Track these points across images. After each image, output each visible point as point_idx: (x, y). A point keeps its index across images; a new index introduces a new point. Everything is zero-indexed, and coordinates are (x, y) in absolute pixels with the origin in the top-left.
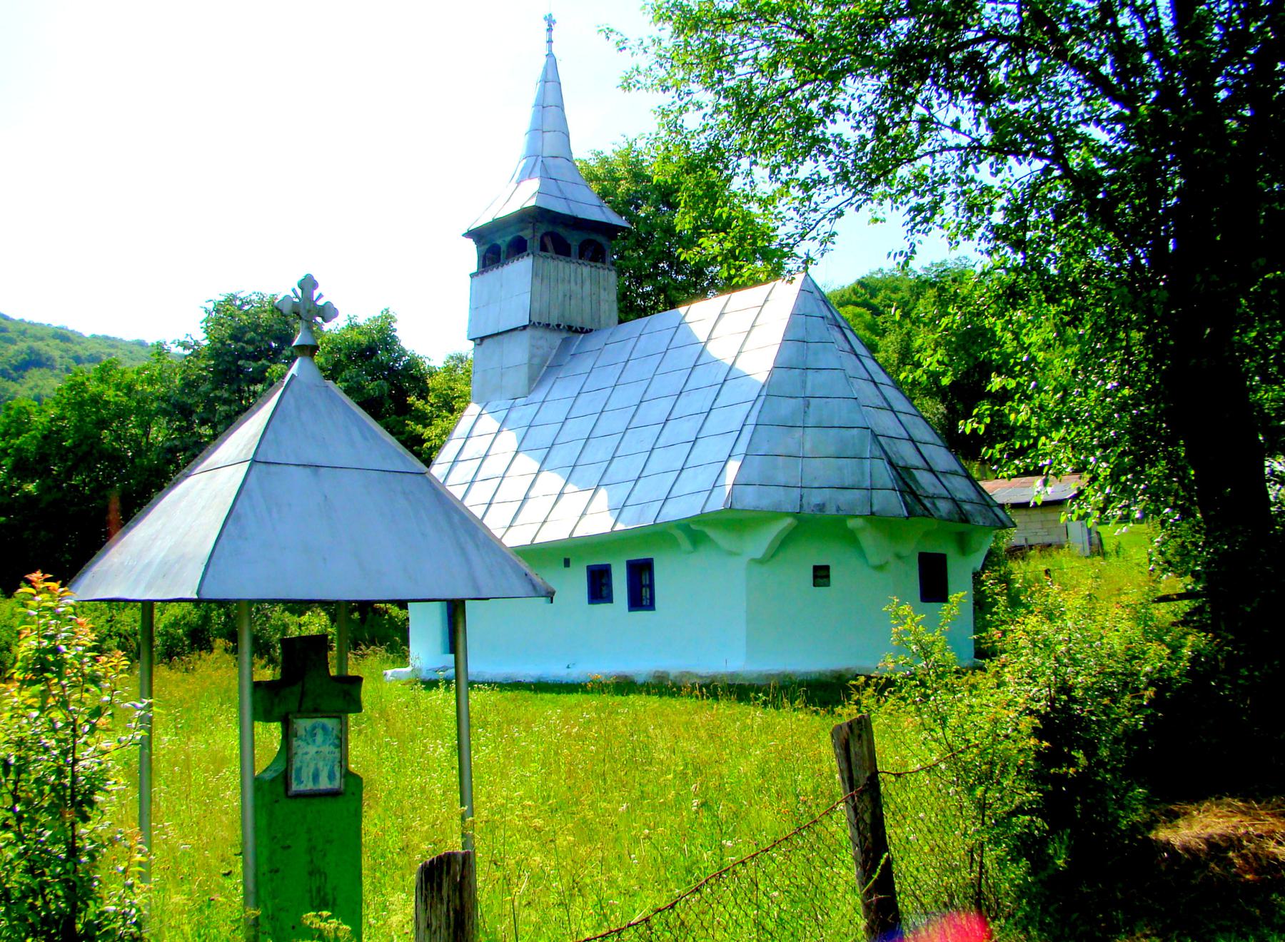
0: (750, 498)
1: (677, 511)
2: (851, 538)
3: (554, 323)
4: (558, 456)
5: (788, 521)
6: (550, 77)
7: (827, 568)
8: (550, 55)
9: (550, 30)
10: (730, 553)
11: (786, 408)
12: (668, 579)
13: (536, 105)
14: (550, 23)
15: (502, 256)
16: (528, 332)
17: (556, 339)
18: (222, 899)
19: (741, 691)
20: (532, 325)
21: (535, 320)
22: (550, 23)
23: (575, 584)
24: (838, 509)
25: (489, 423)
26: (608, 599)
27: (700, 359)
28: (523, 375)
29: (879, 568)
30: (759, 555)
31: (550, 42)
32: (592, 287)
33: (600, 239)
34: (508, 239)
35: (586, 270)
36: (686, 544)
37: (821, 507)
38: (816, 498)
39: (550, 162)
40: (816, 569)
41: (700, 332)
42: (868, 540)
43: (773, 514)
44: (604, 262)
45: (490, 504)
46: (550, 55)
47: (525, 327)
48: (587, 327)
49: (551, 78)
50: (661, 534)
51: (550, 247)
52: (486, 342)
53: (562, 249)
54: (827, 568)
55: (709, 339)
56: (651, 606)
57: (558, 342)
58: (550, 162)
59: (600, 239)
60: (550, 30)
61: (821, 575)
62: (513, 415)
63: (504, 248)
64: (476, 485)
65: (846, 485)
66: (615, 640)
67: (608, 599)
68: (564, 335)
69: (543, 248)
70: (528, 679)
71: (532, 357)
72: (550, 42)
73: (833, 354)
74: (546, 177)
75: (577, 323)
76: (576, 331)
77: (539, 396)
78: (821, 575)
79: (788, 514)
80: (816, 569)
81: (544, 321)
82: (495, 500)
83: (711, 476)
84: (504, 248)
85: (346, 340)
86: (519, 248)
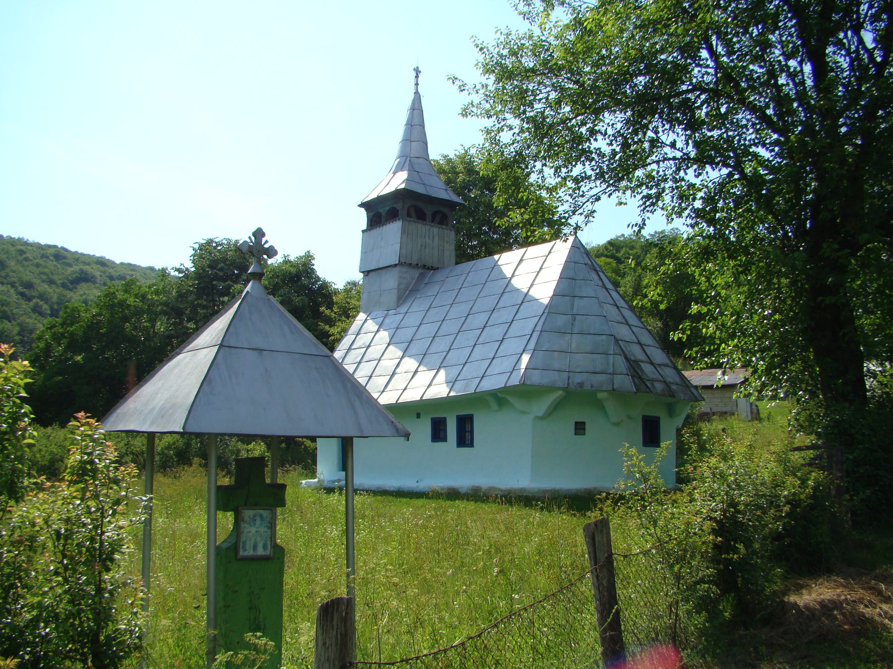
1: (489, 384)
2: (600, 405)
4: (413, 349)
6: (416, 107)
7: (584, 423)
8: (417, 93)
9: (417, 77)
10: (523, 413)
11: (561, 321)
12: (481, 429)
14: (417, 71)
17: (416, 273)
20: (400, 264)
21: (403, 260)
22: (417, 71)
26: (444, 439)
27: (507, 286)
28: (394, 296)
29: (617, 424)
31: (417, 84)
32: (439, 240)
33: (446, 210)
34: (387, 208)
35: (436, 230)
36: (494, 405)
37: (581, 385)
38: (578, 379)
40: (576, 423)
41: (507, 271)
42: (610, 406)
44: (447, 225)
45: (371, 377)
46: (417, 93)
47: (396, 265)
48: (436, 266)
49: (416, 108)
50: (479, 399)
51: (413, 214)
53: (421, 216)
54: (584, 423)
55: (513, 276)
56: (471, 445)
58: (415, 161)
59: (446, 210)
60: (417, 77)
61: (580, 428)
62: (387, 321)
65: (597, 371)
67: (444, 439)
68: (421, 271)
69: (409, 215)
71: (399, 284)
72: (417, 84)
75: (429, 264)
76: (428, 268)
77: (403, 309)
78: (580, 428)
79: (559, 388)
80: (576, 423)
81: (408, 261)
86: (393, 215)
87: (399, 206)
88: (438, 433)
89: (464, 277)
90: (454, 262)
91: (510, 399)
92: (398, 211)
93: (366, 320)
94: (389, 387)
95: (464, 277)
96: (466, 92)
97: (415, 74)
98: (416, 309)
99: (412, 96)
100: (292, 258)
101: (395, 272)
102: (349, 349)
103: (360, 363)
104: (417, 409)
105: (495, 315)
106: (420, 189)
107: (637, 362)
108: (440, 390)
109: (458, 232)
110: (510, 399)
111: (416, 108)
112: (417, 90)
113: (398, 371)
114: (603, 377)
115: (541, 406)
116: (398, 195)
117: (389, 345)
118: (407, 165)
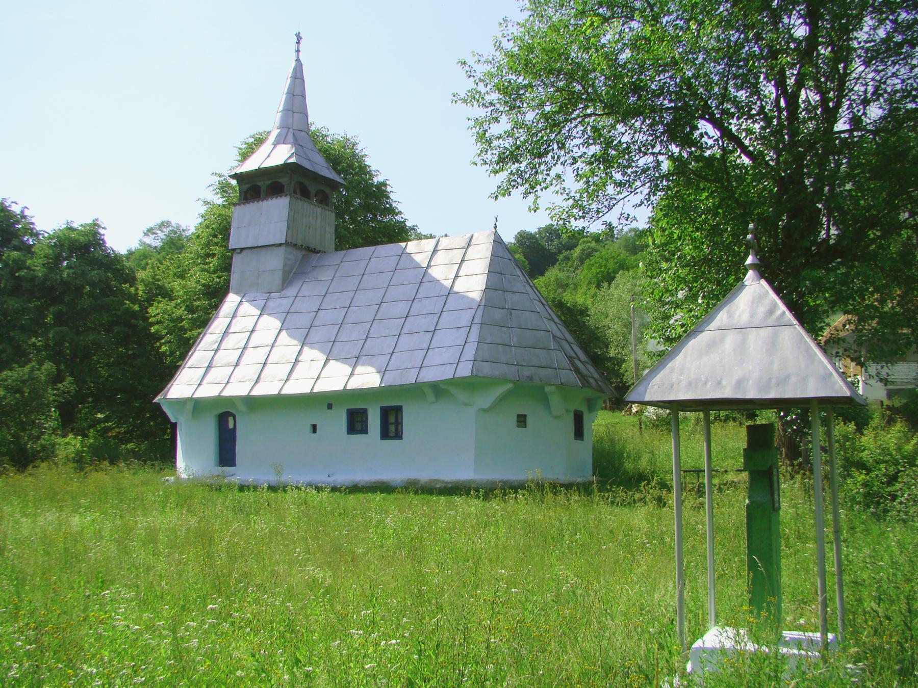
0: (487, 369)
1: (431, 375)
2: (544, 400)
3: (299, 244)
4: (316, 335)
5: (510, 385)
6: (298, 75)
7: (525, 416)
8: (298, 60)
9: (298, 43)
10: (465, 404)
11: (498, 315)
12: (412, 419)
13: (288, 93)
14: (299, 38)
15: (262, 194)
16: (283, 249)
17: (299, 254)
18: (850, 666)
19: (488, 491)
20: (287, 244)
21: (289, 240)
22: (299, 38)
23: (340, 420)
24: (541, 380)
25: (248, 308)
26: (365, 431)
27: (424, 276)
28: (278, 277)
29: (557, 417)
30: (487, 405)
31: (298, 51)
32: (321, 222)
33: (327, 190)
34: (268, 183)
35: (319, 210)
36: (431, 397)
37: (530, 378)
38: (527, 372)
39: (298, 133)
40: (519, 416)
41: (421, 259)
42: (555, 400)
43: (502, 380)
44: (327, 205)
45: (265, 364)
46: (298, 60)
47: (281, 245)
48: (318, 248)
49: (298, 76)
50: (416, 391)
51: (298, 191)
52: (245, 252)
53: (304, 193)
54: (525, 416)
55: (429, 266)
56: (398, 436)
57: (300, 257)
58: (298, 133)
59: (327, 190)
60: (298, 43)
61: (522, 420)
62: (271, 304)
63: (263, 188)
64: (248, 351)
65: (543, 365)
66: (372, 459)
67: (365, 431)
68: (304, 253)
69: (295, 192)
70: (363, 484)
71: (284, 266)
72: (298, 51)
73: (519, 281)
74: (296, 143)
75: (312, 246)
76: (311, 251)
77: (291, 291)
78: (522, 420)
79: (511, 381)
80: (519, 416)
81: (294, 242)
82: (269, 361)
83: (448, 356)
84: (263, 188)
85: (69, 239)
86: (276, 190)
87: (284, 181)
88: (356, 422)
89: (364, 263)
90: (333, 246)
91: (453, 390)
92: (283, 186)
93: (241, 302)
94: (294, 376)
95: (363, 264)
96: (472, 79)
97: (295, 39)
98: (308, 293)
99: (294, 64)
100: (75, 225)
101: (282, 250)
102: (226, 333)
103: (245, 348)
104: (328, 401)
105: (416, 304)
106: (307, 165)
107: (572, 357)
108: (367, 378)
109: (340, 215)
110: (453, 390)
111: (298, 76)
112: (298, 57)
113: (300, 358)
114: (514, 368)
115: (486, 399)
116: (286, 168)
117: (281, 330)
118: (290, 136)
